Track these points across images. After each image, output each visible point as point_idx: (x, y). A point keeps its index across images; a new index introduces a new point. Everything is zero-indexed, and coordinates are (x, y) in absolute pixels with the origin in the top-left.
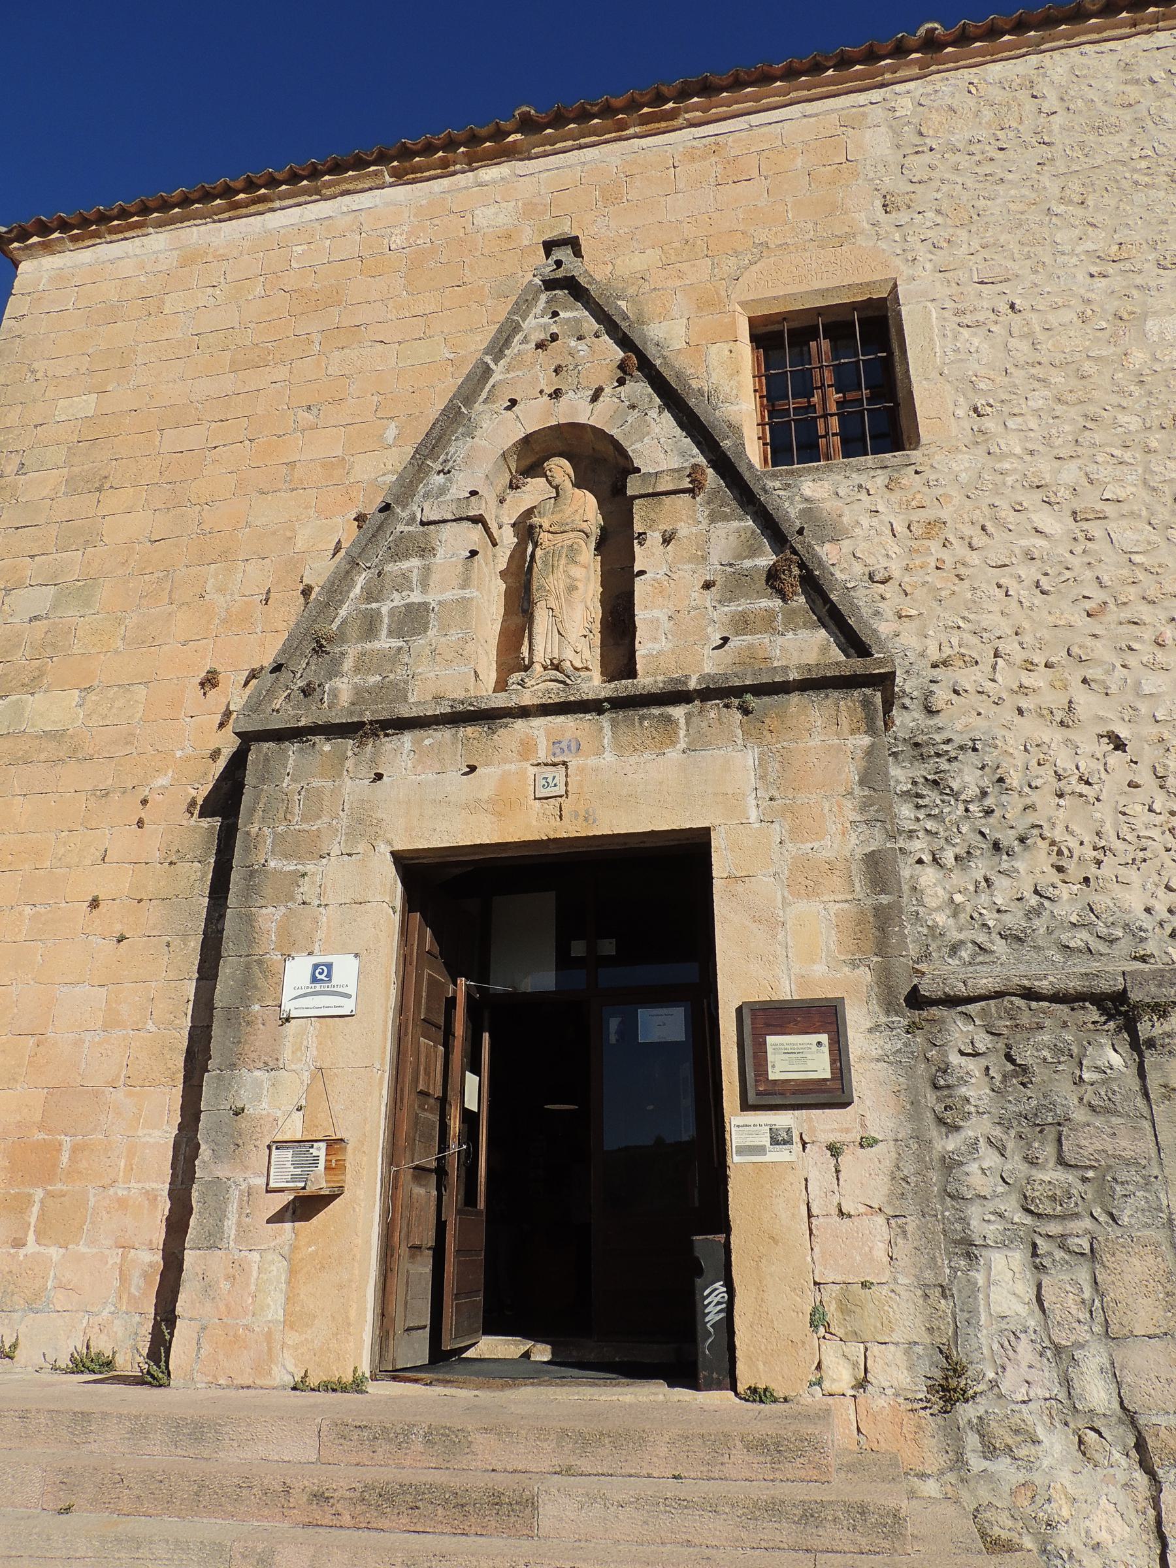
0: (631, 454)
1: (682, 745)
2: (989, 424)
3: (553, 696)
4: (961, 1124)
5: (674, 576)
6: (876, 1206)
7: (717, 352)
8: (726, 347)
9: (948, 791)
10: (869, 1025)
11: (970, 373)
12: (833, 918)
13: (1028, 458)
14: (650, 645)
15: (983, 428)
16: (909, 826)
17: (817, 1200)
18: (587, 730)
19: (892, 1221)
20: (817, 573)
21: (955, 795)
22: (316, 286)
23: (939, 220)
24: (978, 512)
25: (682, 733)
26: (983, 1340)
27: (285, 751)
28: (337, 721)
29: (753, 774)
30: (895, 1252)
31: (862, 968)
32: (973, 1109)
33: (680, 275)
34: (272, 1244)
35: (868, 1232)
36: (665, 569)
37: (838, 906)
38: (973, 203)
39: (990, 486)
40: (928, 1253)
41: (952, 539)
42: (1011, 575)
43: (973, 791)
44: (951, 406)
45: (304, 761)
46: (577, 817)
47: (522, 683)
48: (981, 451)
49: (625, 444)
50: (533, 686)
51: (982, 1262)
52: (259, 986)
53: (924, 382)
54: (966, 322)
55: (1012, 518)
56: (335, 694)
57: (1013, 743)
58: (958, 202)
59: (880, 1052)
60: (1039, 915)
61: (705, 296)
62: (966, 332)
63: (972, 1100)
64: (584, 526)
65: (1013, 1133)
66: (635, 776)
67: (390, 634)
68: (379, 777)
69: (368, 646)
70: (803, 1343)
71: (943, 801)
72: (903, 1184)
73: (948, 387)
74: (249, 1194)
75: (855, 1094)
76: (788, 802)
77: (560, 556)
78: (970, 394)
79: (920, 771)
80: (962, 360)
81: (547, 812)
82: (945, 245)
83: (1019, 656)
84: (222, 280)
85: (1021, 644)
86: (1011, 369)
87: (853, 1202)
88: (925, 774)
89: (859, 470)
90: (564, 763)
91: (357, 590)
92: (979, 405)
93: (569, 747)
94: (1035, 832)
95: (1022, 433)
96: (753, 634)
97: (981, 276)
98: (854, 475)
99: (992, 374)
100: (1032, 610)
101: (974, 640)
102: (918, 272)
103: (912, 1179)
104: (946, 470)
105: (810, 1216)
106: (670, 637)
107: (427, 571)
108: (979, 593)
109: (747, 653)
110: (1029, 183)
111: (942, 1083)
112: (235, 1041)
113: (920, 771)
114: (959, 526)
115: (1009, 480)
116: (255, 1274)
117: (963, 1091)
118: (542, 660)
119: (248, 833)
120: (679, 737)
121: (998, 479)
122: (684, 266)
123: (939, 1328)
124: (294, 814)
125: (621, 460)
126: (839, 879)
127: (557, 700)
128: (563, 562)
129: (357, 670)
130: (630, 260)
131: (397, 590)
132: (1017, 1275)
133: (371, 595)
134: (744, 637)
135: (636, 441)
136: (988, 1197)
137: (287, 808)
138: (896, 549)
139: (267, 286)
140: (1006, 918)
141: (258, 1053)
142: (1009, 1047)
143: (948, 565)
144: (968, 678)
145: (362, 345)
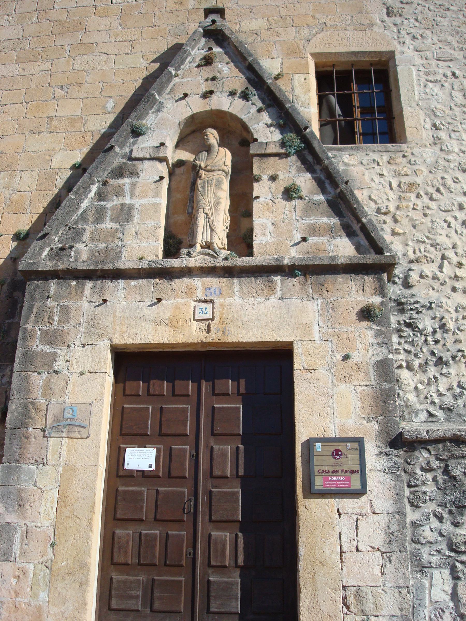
0: (252, 130)
1: (279, 293)
2: (443, 135)
3: (207, 263)
4: (421, 505)
5: (276, 201)
6: (377, 547)
7: (298, 79)
8: (303, 76)
9: (417, 329)
10: (376, 452)
11: (433, 106)
12: (359, 395)
13: (461, 154)
14: (261, 238)
15: (439, 136)
16: (395, 346)
17: (346, 544)
18: (225, 283)
19: (384, 555)
20: (355, 206)
21: (421, 332)
22: (68, 20)
23: (417, 24)
24: (436, 180)
25: (279, 288)
26: (427, 614)
27: (49, 284)
28: (81, 268)
29: (317, 313)
30: (385, 571)
31: (373, 422)
32: (428, 498)
33: (278, 35)
34: (41, 560)
35: (371, 560)
36: (270, 196)
37: (361, 388)
38: (434, 18)
39: (442, 167)
40: (402, 571)
41: (422, 193)
42: (452, 216)
43: (430, 330)
44: (423, 123)
45: (60, 290)
46: (218, 331)
47: (189, 254)
48: (437, 148)
49: (249, 124)
50: (195, 256)
51: (429, 575)
52: (32, 416)
53: (409, 108)
54: (430, 79)
55: (453, 185)
56: (78, 253)
57: (450, 304)
58: (426, 16)
59: (382, 467)
60: (461, 397)
61: (292, 47)
62: (431, 85)
63: (428, 493)
64: (225, 168)
65: (447, 510)
66: (252, 311)
67: (112, 220)
68: (105, 301)
69: (98, 226)
70: (335, 616)
71: (414, 335)
72: (391, 536)
73: (421, 112)
74: (27, 532)
75: (368, 489)
76: (336, 330)
77: (211, 184)
78: (433, 117)
79: (403, 318)
80: (429, 99)
81: (202, 328)
82: (420, 37)
83: (455, 260)
84: (13, 12)
85: (456, 253)
86: (453, 107)
87: (365, 545)
88: (405, 319)
89: (374, 151)
90: (212, 301)
91: (92, 194)
92: (437, 124)
93: (215, 292)
94: (460, 354)
95: (458, 141)
96: (318, 236)
97: (438, 56)
98: (371, 154)
99: (444, 108)
100: (462, 236)
101: (432, 249)
102: (405, 50)
103: (396, 534)
104: (420, 156)
105: (341, 552)
106: (272, 234)
107: (134, 185)
108: (436, 224)
109: (315, 247)
110: (461, 13)
111: (413, 484)
112: (18, 447)
113: (403, 318)
114: (426, 187)
115: (452, 165)
116: (31, 576)
117: (424, 488)
118: (201, 242)
119: (26, 329)
120: (277, 291)
121: (446, 164)
122: (280, 30)
123: (405, 608)
124: (54, 320)
125: (245, 134)
126: (362, 373)
127: (210, 265)
128: (213, 187)
129: (92, 239)
130: (250, 23)
131: (116, 196)
132: (445, 581)
133: (101, 196)
134: (314, 238)
135: (255, 124)
136: (433, 542)
137: (50, 316)
138: (393, 196)
139: (40, 17)
140: (444, 398)
141: (32, 455)
142: (447, 466)
143: (420, 207)
144: (429, 269)
145: (94, 54)
